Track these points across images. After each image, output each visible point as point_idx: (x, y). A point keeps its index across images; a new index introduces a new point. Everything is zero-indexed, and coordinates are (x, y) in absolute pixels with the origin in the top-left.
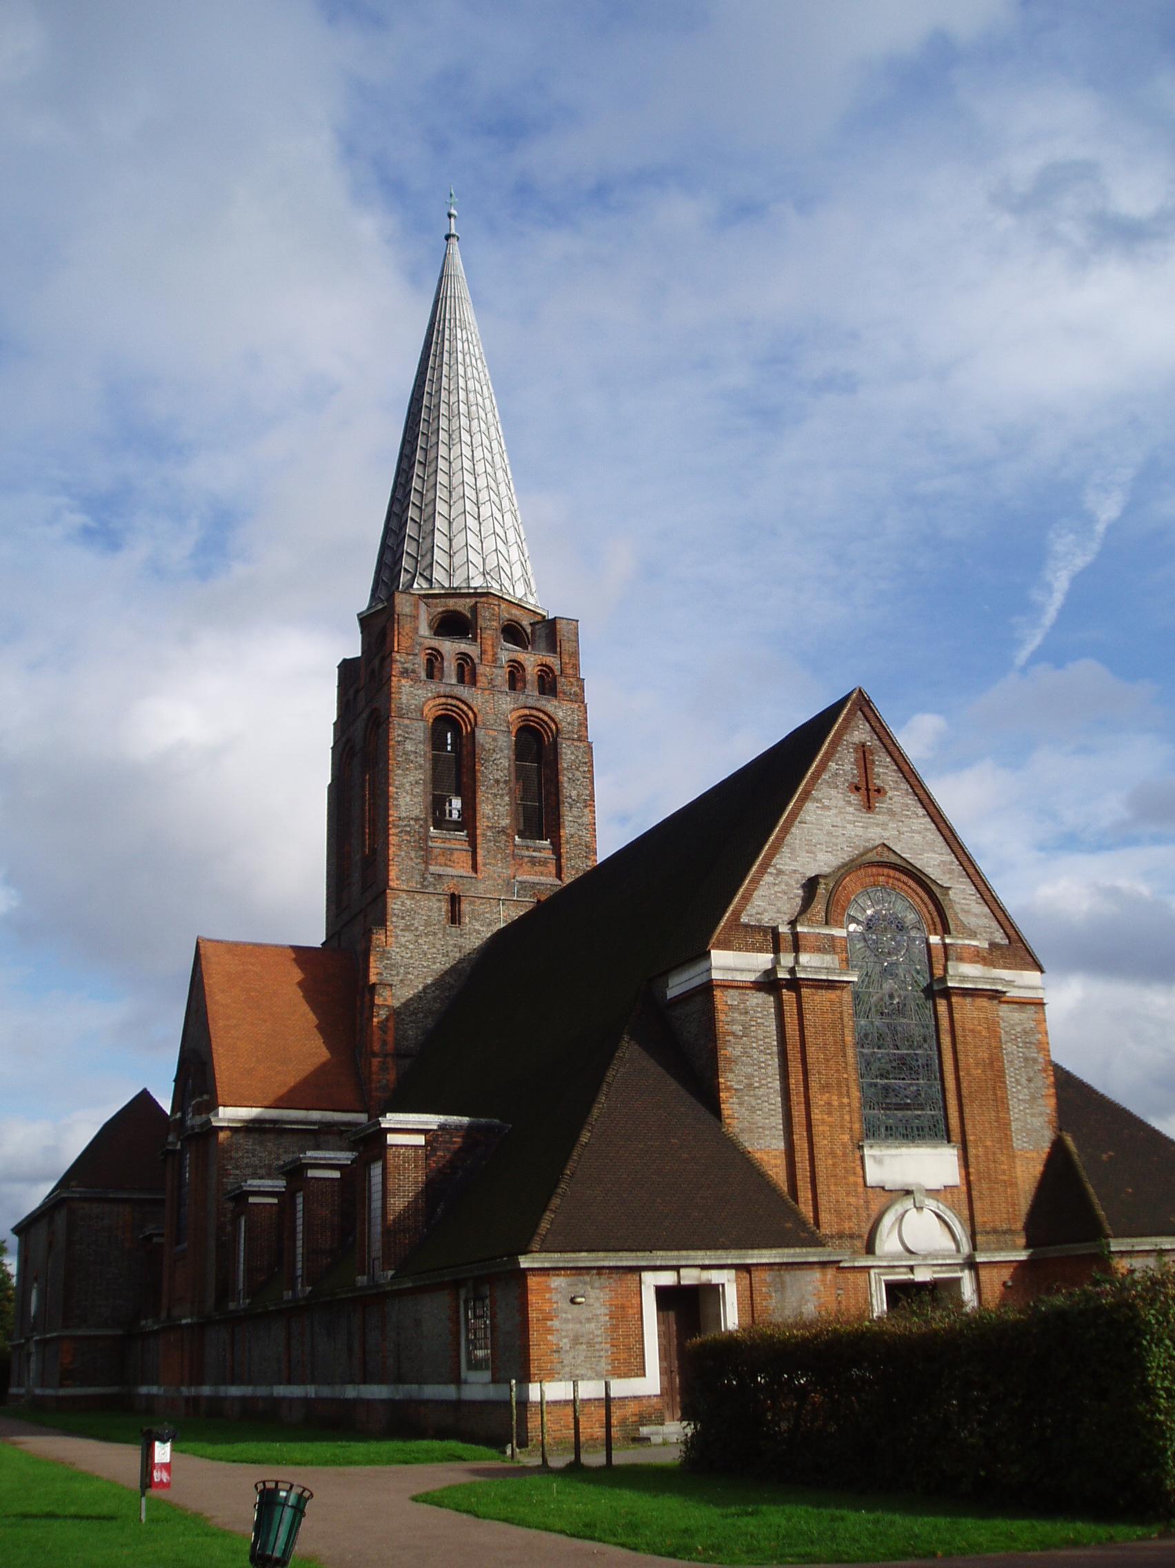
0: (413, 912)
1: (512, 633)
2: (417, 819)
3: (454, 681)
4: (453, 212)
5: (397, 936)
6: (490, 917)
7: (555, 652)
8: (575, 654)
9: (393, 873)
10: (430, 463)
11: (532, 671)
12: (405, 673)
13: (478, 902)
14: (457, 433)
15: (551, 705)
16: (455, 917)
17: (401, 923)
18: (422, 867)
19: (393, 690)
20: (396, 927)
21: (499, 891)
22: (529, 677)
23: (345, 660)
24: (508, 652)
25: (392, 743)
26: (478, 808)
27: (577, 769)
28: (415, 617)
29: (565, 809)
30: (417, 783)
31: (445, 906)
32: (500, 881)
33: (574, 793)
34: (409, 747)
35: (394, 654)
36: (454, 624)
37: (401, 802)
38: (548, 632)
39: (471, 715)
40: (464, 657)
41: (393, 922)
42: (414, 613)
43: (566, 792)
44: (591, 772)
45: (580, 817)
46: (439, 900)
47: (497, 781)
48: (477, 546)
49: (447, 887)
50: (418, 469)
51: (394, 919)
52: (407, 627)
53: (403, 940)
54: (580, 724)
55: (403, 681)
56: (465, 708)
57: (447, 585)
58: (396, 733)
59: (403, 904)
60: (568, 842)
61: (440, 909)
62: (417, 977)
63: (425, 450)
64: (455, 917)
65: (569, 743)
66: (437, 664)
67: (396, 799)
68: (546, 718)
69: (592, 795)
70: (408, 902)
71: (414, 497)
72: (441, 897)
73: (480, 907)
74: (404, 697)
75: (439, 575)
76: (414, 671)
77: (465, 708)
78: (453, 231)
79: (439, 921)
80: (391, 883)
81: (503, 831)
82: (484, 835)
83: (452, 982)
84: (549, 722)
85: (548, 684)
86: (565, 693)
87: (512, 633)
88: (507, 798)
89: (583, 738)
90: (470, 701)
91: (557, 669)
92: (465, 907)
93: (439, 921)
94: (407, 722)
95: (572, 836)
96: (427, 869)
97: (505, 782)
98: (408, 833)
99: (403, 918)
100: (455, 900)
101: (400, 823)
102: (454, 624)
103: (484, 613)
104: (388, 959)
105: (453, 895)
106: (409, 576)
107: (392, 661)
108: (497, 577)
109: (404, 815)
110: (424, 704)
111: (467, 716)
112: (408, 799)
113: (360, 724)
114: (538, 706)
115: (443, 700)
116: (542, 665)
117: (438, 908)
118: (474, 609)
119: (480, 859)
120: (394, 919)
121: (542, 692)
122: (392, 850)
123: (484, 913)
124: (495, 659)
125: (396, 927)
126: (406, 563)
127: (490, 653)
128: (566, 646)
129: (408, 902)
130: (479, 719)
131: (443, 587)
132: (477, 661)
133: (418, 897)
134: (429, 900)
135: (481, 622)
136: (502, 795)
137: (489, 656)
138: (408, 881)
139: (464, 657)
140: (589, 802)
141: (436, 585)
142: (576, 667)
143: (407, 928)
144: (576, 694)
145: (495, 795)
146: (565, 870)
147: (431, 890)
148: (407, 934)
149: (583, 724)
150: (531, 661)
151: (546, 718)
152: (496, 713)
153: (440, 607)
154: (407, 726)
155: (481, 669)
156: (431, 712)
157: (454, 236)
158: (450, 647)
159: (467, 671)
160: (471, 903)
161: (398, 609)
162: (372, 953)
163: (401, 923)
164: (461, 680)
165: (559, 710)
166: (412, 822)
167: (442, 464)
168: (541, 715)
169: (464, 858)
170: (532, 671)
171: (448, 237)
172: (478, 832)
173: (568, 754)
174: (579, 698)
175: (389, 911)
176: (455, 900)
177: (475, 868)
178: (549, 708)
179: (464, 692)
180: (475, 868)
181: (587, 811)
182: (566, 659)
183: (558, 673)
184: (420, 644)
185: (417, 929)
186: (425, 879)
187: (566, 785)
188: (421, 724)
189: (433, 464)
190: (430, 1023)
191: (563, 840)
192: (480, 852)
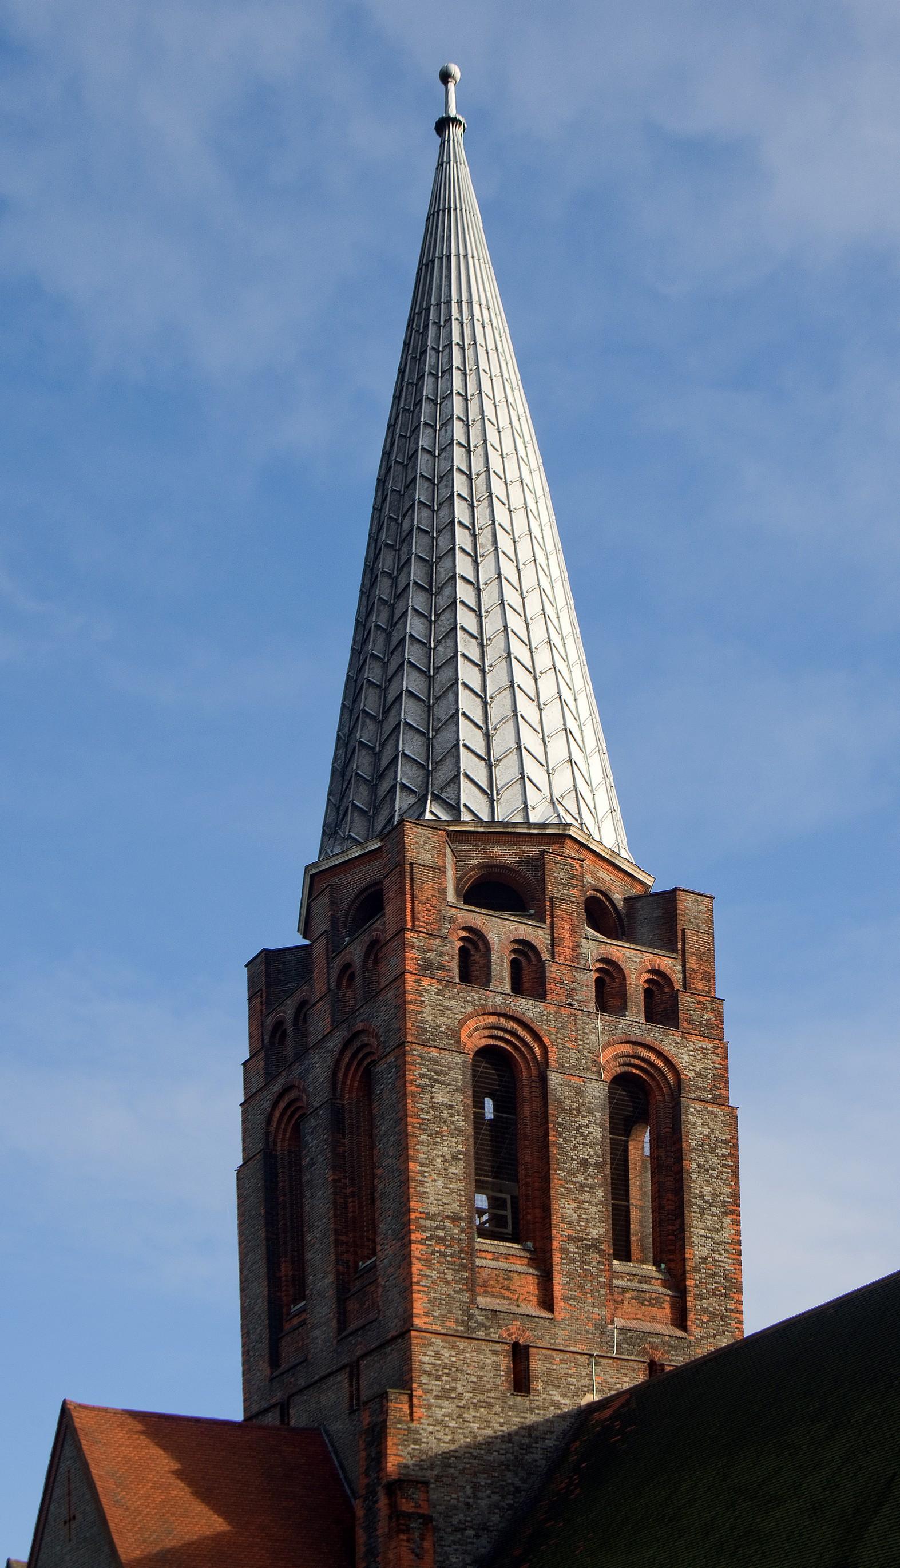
0: (453, 1370)
1: (600, 914)
2: (455, 1219)
3: (507, 988)
4: (455, 70)
5: (429, 1407)
6: (580, 1380)
7: (674, 950)
8: (707, 956)
9: (420, 1304)
10: (439, 586)
11: (636, 981)
12: (427, 968)
13: (558, 1357)
14: (488, 532)
15: (669, 1042)
16: (521, 1382)
17: (435, 1386)
18: (465, 1297)
19: (409, 997)
20: (427, 1392)
21: (588, 1341)
22: (630, 990)
23: (265, 951)
24: (594, 946)
25: (410, 1088)
26: (554, 1205)
27: (713, 1151)
28: (441, 870)
29: (692, 1216)
30: (455, 1158)
31: (504, 1363)
32: (590, 1327)
33: (708, 1190)
34: (440, 1096)
35: (408, 935)
36: (502, 888)
37: (429, 1189)
38: (654, 916)
39: (537, 1050)
40: (524, 949)
41: (425, 1386)
42: (439, 862)
43: (695, 1188)
44: (734, 1156)
45: (717, 1231)
46: (495, 1352)
47: (584, 1163)
48: (538, 750)
49: (513, 1331)
50: (416, 600)
51: (424, 1379)
52: (426, 890)
53: (439, 1414)
54: (716, 1077)
55: (425, 983)
56: (528, 1038)
57: (485, 817)
58: (416, 1073)
59: (438, 1355)
60: (697, 1270)
61: (496, 1367)
62: (462, 1472)
63: (428, 564)
64: (521, 1382)
65: (700, 1106)
66: (477, 957)
67: (422, 1183)
68: (660, 1063)
69: (735, 1196)
70: (446, 1353)
71: (412, 653)
72: (498, 1347)
73: (560, 1366)
74: (427, 1010)
75: (469, 797)
76: (441, 967)
77: (528, 1038)
78: (453, 112)
79: (496, 1387)
80: (417, 1321)
81: (594, 1246)
82: (564, 1251)
83: (517, 1482)
84: (665, 1070)
85: (662, 1004)
86: (691, 1022)
87: (600, 914)
88: (600, 1193)
89: (721, 1100)
90: (536, 1025)
91: (677, 978)
92: (537, 1365)
93: (496, 1387)
94: (434, 1053)
95: (704, 1260)
96: (473, 1301)
97: (597, 1165)
98: (441, 1240)
99: (438, 1378)
100: (520, 1354)
101: (428, 1223)
102: (502, 888)
103: (556, 875)
104: (416, 1442)
105: (516, 1345)
106: (412, 800)
107: (403, 945)
108: (574, 810)
109: (433, 1210)
110: (462, 1023)
111: (531, 1049)
112: (440, 1183)
113: (317, 1070)
114: (648, 1039)
115: (492, 1020)
116: (652, 971)
117: (494, 1364)
118: (538, 864)
119: (558, 1291)
120: (424, 1379)
121: (651, 1017)
122: (417, 1266)
123: (568, 1376)
124: (577, 957)
125: (427, 1392)
126: (405, 774)
127: (568, 943)
128: (694, 941)
129: (446, 1353)
130: (552, 1056)
131: (479, 820)
132: (545, 956)
133: (461, 1344)
134: (479, 1351)
135: (551, 889)
136: (592, 1187)
137: (565, 951)
138: (443, 1318)
139: (524, 949)
140: (732, 1207)
141: (466, 816)
142: (709, 977)
143: (444, 1395)
144: (709, 1025)
145: (582, 1187)
146: (692, 1316)
147: (481, 1334)
148: (445, 1403)
149: (722, 1078)
150: (636, 961)
151: (660, 1063)
152: (584, 1054)
153: (477, 857)
154: (434, 1061)
155: (553, 971)
156: (474, 1039)
157: (455, 121)
158: (502, 931)
159: (528, 973)
160: (547, 1359)
161: (411, 854)
162: (391, 1431)
163: (435, 1386)
164: (517, 988)
165: (685, 1053)
166: (448, 1223)
167: (464, 592)
168: (652, 1057)
169: (528, 1285)
170: (636, 981)
171: (443, 125)
172: (556, 1244)
173: (698, 1124)
174: (714, 1031)
175: (416, 1364)
176: (520, 1354)
177: (547, 1302)
178: (668, 1047)
179: (526, 1007)
180: (547, 1302)
181: (727, 1220)
182: (692, 963)
183: (678, 986)
184: (452, 920)
185: (460, 1397)
186: (471, 1317)
187: (694, 1176)
188: (458, 1058)
189: (447, 591)
190: (484, 1545)
191: (690, 1265)
192: (559, 1281)
